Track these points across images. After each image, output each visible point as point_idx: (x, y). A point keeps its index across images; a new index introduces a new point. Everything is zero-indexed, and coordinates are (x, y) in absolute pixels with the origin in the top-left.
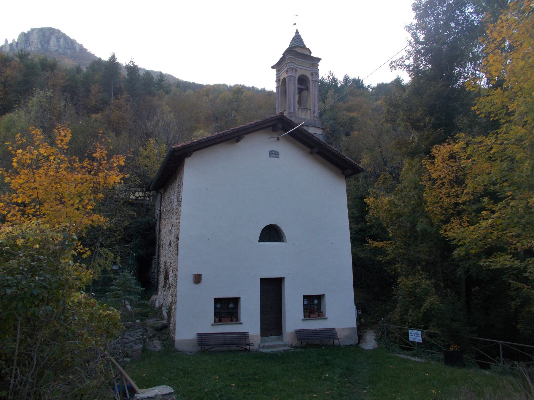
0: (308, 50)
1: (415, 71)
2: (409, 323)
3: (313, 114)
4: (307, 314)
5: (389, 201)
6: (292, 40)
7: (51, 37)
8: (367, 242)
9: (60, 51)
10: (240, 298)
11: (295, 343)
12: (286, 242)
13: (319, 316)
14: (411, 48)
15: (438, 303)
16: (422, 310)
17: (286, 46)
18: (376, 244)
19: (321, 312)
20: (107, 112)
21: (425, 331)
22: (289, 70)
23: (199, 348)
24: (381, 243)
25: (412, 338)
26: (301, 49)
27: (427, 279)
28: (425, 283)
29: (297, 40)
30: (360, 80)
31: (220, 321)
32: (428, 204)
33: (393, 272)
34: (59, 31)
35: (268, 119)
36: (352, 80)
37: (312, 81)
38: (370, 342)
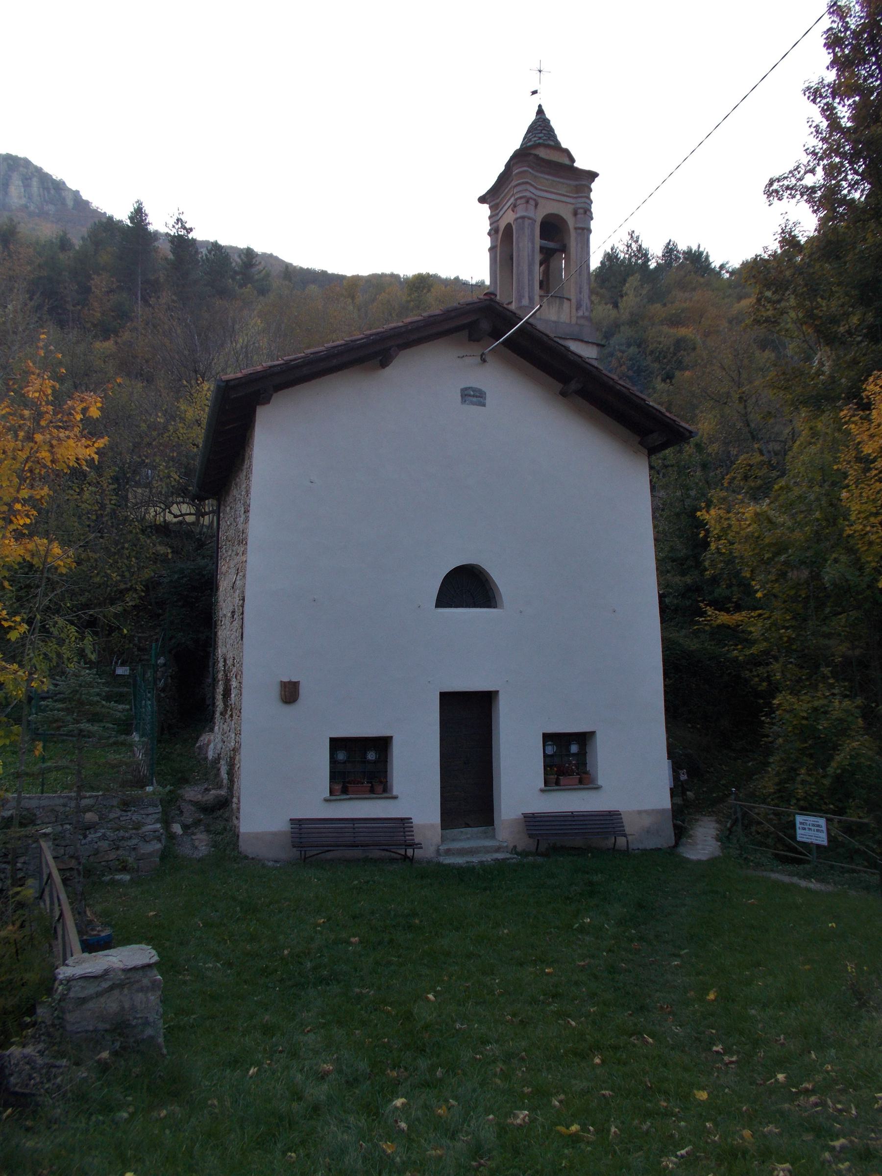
0: (567, 152)
1: (827, 200)
2: (798, 800)
3: (577, 309)
4: (553, 777)
5: (757, 514)
6: (529, 131)
7: (10, 177)
8: (703, 614)
9: (32, 207)
10: (392, 737)
11: (524, 843)
12: (502, 607)
13: (581, 782)
14: (821, 143)
15: (870, 753)
16: (830, 770)
17: (516, 143)
18: (723, 618)
19: (586, 773)
20: (126, 336)
21: (837, 818)
22: (519, 202)
23: (295, 853)
24: (737, 617)
25: (802, 835)
26: (548, 151)
27: (846, 696)
28: (840, 707)
29: (541, 129)
30: (701, 253)
31: (345, 791)
32: (853, 518)
33: (765, 684)
34: (26, 162)
35: (456, 309)
36: (684, 253)
37: (576, 229)
38: (704, 842)
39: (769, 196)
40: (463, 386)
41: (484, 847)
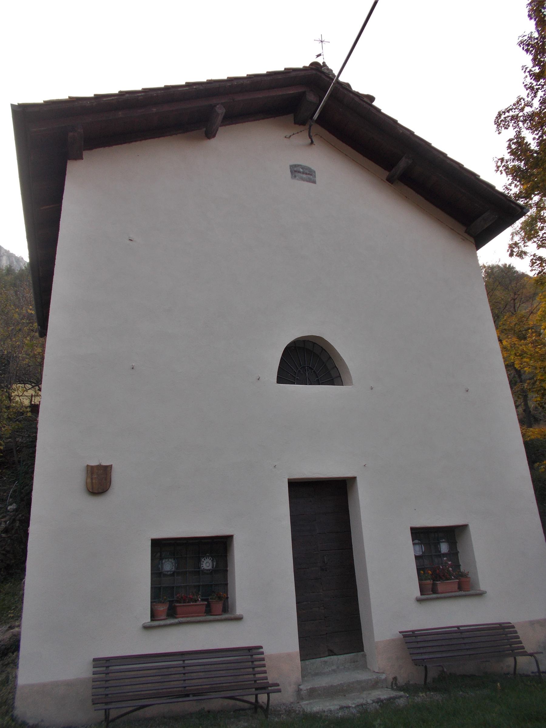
12: (350, 383)
13: (460, 588)
19: (464, 575)
31: (172, 613)
39: (498, 125)
40: (292, 164)
41: (359, 682)
